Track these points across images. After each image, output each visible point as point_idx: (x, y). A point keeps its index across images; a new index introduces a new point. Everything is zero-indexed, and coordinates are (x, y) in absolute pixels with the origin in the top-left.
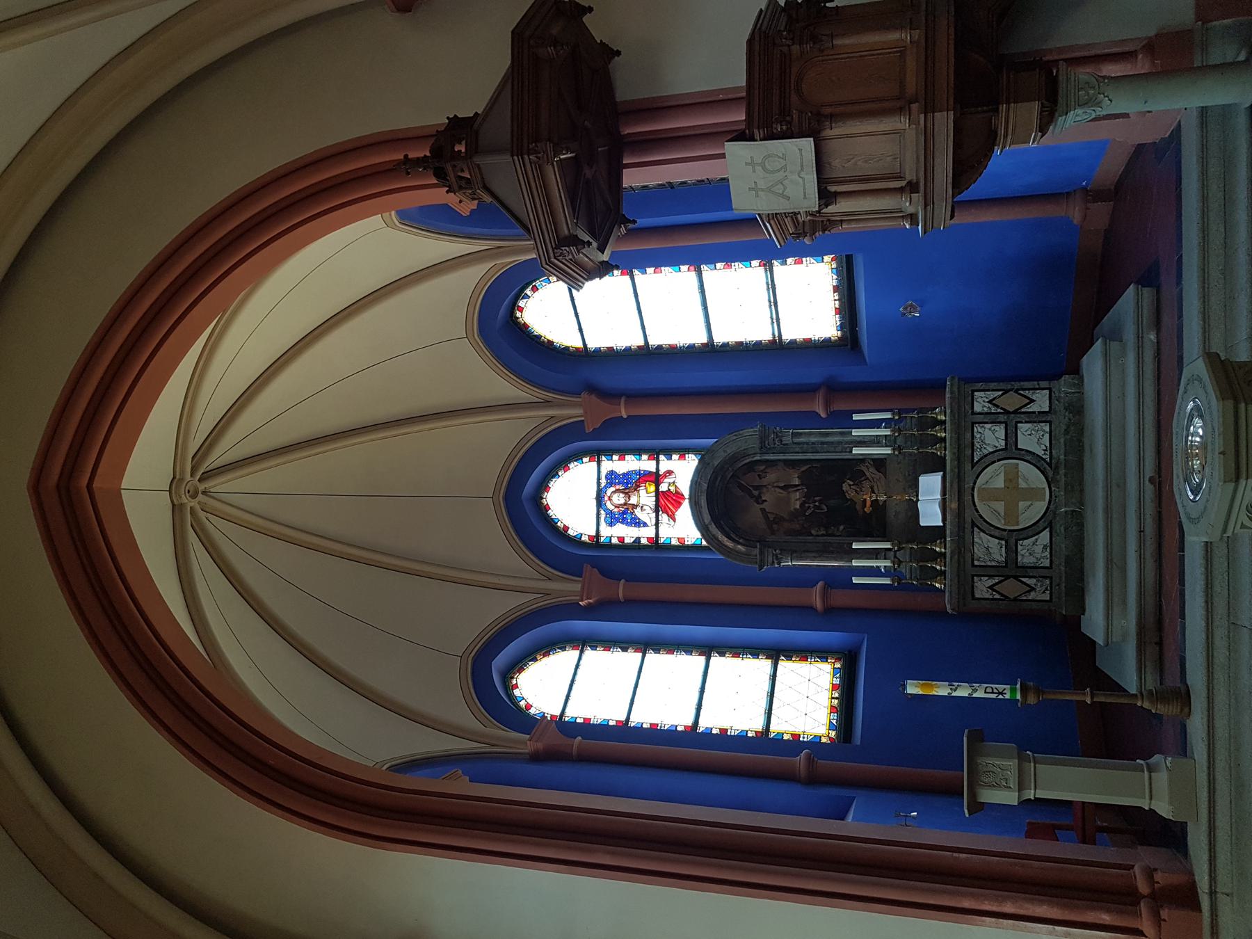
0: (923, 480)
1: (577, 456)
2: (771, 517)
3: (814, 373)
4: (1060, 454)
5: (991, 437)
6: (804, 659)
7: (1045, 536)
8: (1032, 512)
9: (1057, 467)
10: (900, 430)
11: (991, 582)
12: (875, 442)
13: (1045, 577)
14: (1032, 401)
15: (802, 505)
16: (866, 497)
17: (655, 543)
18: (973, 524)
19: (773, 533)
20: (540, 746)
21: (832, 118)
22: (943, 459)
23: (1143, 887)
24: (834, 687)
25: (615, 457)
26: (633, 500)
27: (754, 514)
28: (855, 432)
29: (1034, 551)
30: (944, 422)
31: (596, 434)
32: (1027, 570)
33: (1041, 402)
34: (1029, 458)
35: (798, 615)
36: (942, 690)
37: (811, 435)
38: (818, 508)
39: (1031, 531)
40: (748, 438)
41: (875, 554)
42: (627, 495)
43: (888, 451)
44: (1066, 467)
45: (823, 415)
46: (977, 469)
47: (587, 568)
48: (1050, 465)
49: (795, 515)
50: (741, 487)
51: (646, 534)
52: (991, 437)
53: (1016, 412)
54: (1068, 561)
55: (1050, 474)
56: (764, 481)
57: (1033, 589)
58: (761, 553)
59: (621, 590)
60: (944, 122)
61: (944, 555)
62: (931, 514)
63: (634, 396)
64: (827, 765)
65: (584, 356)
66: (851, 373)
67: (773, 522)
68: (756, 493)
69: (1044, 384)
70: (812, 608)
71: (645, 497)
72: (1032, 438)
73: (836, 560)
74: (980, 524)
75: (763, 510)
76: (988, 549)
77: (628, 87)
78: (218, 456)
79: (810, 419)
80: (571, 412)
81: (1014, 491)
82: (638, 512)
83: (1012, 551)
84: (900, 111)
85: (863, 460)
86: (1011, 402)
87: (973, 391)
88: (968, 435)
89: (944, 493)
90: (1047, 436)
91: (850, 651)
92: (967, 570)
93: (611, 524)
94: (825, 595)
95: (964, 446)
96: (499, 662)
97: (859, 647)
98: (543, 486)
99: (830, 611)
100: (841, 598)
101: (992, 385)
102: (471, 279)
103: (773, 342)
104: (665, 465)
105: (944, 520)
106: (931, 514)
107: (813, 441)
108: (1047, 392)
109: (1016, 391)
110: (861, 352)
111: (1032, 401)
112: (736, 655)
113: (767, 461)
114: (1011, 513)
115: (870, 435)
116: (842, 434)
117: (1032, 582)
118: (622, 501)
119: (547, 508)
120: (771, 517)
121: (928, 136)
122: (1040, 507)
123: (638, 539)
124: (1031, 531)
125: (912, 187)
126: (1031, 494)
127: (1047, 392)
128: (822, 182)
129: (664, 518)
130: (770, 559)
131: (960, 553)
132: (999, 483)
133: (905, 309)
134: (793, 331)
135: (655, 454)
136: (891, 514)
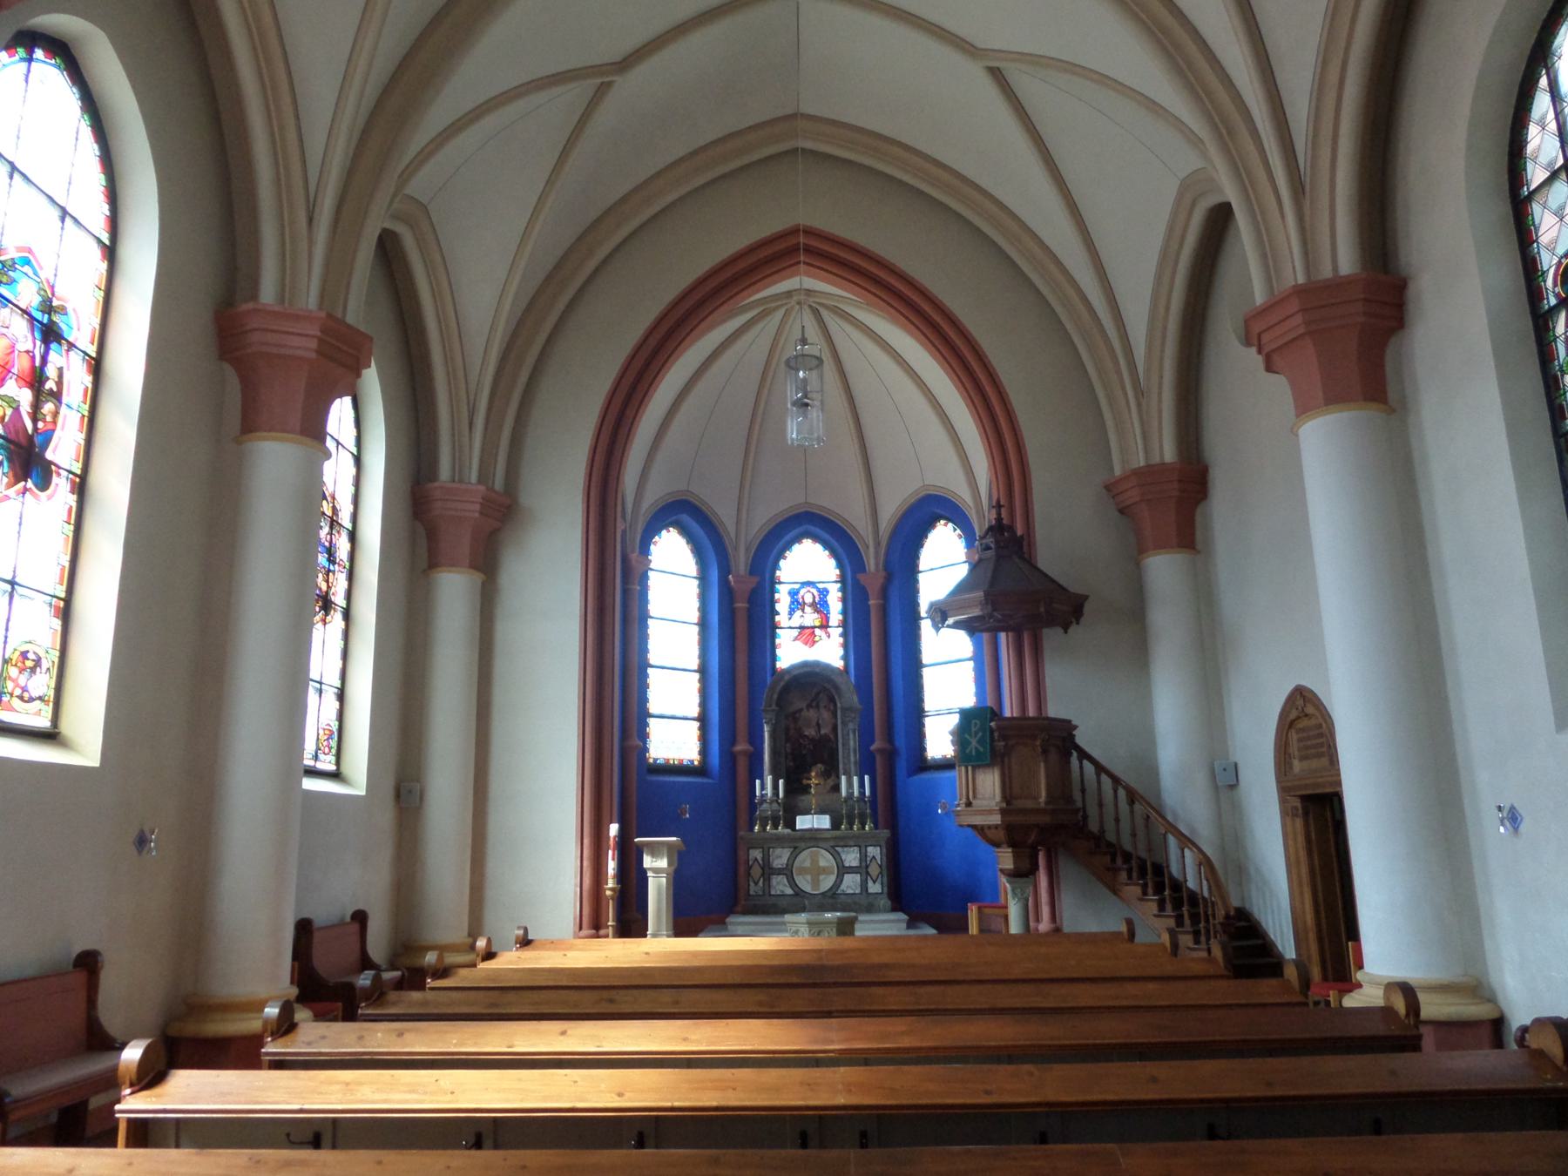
1: (840, 565)
3: (901, 742)
5: (851, 857)
7: (789, 891)
8: (805, 884)
17: (775, 627)
26: (807, 609)
29: (780, 885)
31: (856, 582)
32: (768, 880)
35: (729, 736)
42: (813, 605)
45: (873, 748)
47: (755, 580)
49: (799, 731)
50: (818, 694)
52: (851, 857)
54: (774, 905)
56: (823, 711)
59: (741, 605)
62: (803, 822)
63: (884, 610)
64: (634, 761)
66: (902, 765)
67: (795, 716)
71: (811, 618)
78: (825, 313)
79: (866, 736)
81: (817, 871)
82: (799, 613)
83: (780, 872)
86: (874, 870)
92: (767, 844)
95: (845, 842)
96: (685, 518)
98: (816, 539)
102: (963, 494)
106: (803, 822)
107: (849, 747)
114: (803, 871)
115: (852, 785)
121: (990, 812)
122: (807, 888)
125: (969, 804)
126: (816, 883)
129: (796, 632)
132: (822, 863)
135: (844, 624)
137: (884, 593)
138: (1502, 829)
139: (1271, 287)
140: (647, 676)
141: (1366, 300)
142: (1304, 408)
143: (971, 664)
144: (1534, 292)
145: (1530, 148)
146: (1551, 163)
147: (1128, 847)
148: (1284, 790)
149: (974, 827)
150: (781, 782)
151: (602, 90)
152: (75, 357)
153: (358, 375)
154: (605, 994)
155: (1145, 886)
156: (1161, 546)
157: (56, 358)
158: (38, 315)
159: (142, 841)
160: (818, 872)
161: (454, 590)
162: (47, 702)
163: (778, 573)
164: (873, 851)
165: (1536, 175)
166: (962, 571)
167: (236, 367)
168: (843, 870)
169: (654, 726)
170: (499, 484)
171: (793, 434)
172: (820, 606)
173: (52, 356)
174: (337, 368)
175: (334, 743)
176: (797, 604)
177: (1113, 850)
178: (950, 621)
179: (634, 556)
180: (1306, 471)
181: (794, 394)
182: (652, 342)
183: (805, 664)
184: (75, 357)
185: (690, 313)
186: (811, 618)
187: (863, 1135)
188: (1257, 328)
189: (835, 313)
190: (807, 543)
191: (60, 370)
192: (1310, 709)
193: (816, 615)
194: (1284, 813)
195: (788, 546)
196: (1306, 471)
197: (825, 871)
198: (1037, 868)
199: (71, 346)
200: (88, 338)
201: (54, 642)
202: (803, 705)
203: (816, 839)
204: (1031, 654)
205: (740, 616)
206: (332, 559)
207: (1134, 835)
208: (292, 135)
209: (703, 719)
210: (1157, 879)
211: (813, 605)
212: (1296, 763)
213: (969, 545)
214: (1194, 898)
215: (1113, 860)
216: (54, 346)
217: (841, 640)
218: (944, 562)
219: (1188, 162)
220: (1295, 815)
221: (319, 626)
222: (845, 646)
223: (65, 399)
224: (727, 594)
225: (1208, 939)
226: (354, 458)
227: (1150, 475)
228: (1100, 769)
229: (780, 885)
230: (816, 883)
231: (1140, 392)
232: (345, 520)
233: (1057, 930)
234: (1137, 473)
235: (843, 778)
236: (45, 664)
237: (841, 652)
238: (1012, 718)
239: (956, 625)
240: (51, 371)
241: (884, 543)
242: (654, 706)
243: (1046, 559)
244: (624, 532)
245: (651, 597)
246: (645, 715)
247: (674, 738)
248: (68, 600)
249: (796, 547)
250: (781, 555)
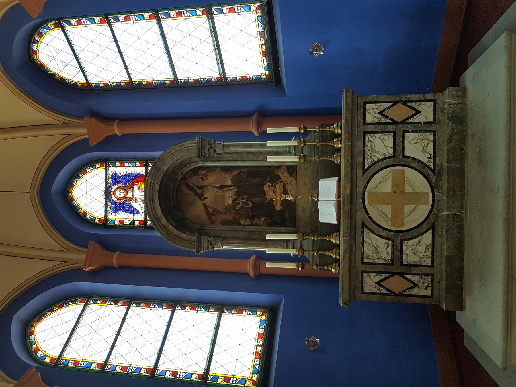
1: (91, 163)
2: (211, 211)
3: (250, 102)
4: (442, 160)
5: (381, 145)
6: (240, 312)
8: (416, 215)
9: (440, 174)
10: (305, 142)
11: (378, 278)
12: (287, 151)
13: (427, 275)
14: (418, 112)
15: (234, 201)
16: (275, 195)
18: (364, 225)
19: (212, 223)
22: (339, 166)
24: (260, 336)
25: (118, 164)
26: (130, 195)
28: (269, 143)
29: (417, 251)
30: (339, 135)
34: (413, 165)
37: (238, 147)
38: (246, 203)
39: (415, 232)
40: (188, 150)
41: (286, 243)
42: (126, 191)
43: (295, 159)
44: (450, 174)
46: (368, 174)
48: (433, 171)
49: (228, 209)
50: (189, 187)
52: (381, 145)
53: (403, 122)
54: (449, 261)
55: (434, 179)
56: (206, 183)
57: (415, 285)
58: (199, 240)
59: (115, 259)
61: (338, 246)
62: (328, 214)
63: (124, 120)
65: (88, 90)
66: (275, 103)
68: (199, 192)
69: (429, 96)
70: (247, 274)
73: (256, 245)
74: (369, 225)
75: (205, 205)
76: (377, 248)
79: (247, 136)
80: (80, 132)
81: (399, 196)
83: (398, 250)
85: (278, 167)
86: (400, 113)
87: (365, 103)
88: (361, 144)
89: (339, 195)
90: (431, 145)
91: (273, 307)
92: (358, 268)
93: (115, 212)
97: (279, 304)
101: (382, 98)
103: (219, 80)
105: (338, 220)
106: (328, 214)
107: (237, 152)
108: (432, 104)
109: (404, 103)
110: (284, 91)
111: (418, 112)
112: (193, 308)
113: (208, 167)
114: (397, 215)
115: (281, 148)
116: (261, 145)
117: (415, 279)
118: (122, 195)
119: (72, 199)
120: (211, 211)
122: (423, 210)
123: (133, 222)
124: (415, 232)
126: (416, 198)
127: (432, 104)
130: (206, 245)
131: (351, 251)
132: (387, 188)
133: (313, 49)
134: (235, 71)
136: (299, 209)
137: (107, 119)
150: (269, 237)
160: (400, 194)
164: (372, 114)
168: (399, 158)
187: (397, 185)
197: (398, 185)
202: (199, 203)
203: (352, 195)
224: (101, 273)
230: (416, 198)
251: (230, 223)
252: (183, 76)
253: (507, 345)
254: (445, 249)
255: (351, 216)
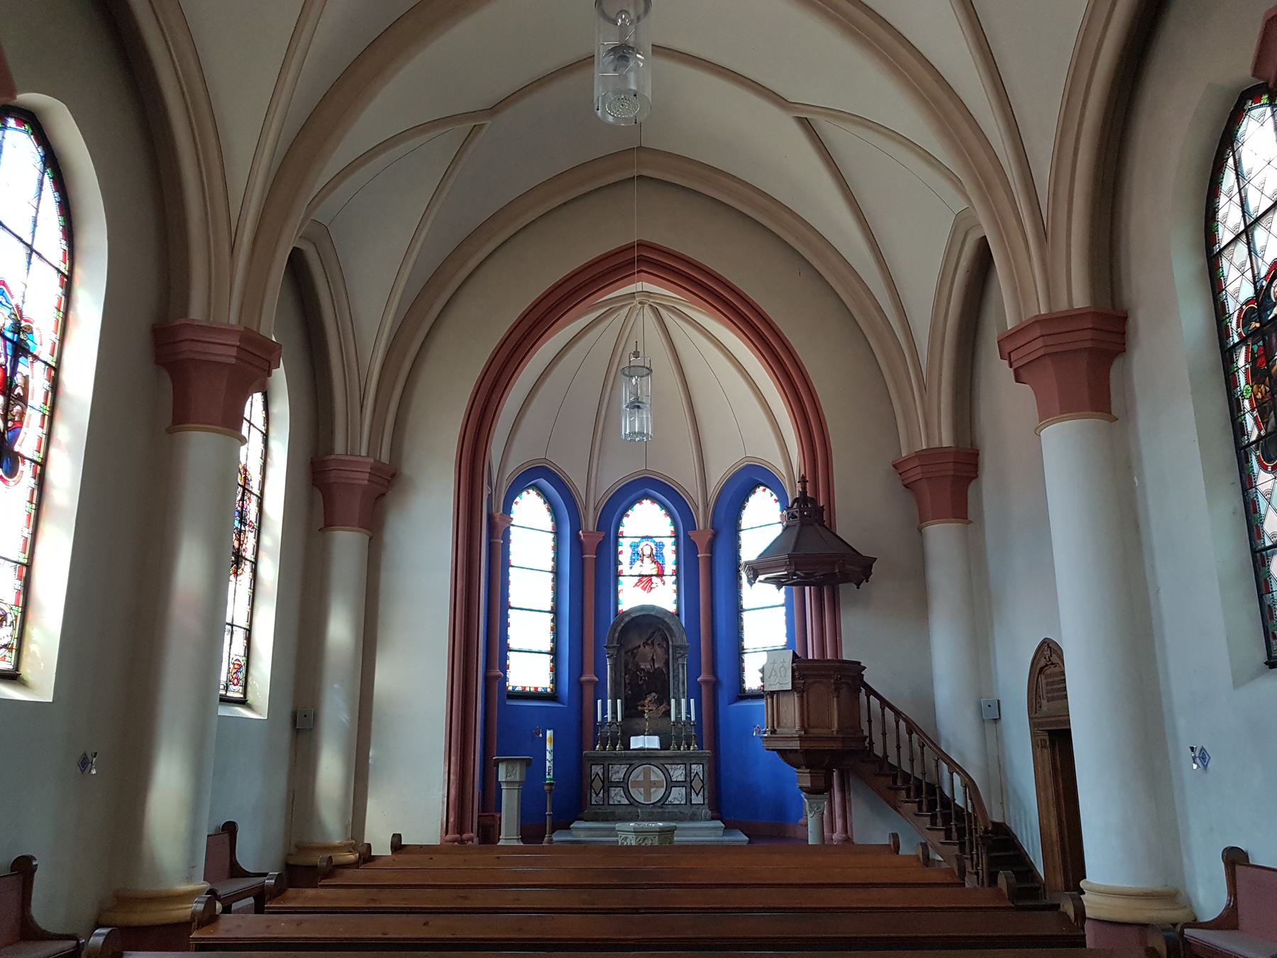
0: (657, 738)
4: (670, 809)
5: (678, 774)
17: (618, 575)
20: (497, 520)
21: (801, 698)
23: (465, 836)
27: (637, 641)
29: (617, 796)
33: (697, 800)
35: (578, 665)
36: (549, 747)
37: (683, 674)
39: (628, 794)
41: (615, 712)
42: (651, 556)
49: (637, 666)
51: (624, 568)
52: (678, 774)
59: (590, 556)
60: (796, 745)
62: (636, 742)
63: (711, 561)
65: (736, 529)
66: (724, 695)
67: (633, 653)
70: (581, 675)
71: (649, 568)
72: (677, 795)
76: (618, 773)
77: (846, 590)
79: (694, 670)
81: (649, 786)
82: (638, 563)
83: (617, 784)
84: (802, 726)
85: (669, 704)
86: (697, 784)
92: (606, 761)
94: (590, 681)
95: (674, 760)
96: (543, 482)
98: (655, 500)
99: (581, 685)
100: (589, 692)
102: (779, 466)
104: (670, 580)
106: (636, 742)
107: (681, 674)
110: (736, 701)
114: (637, 784)
115: (683, 709)
119: (640, 503)
121: (791, 738)
123: (621, 563)
124: (628, 794)
125: (773, 732)
126: (648, 795)
128: (778, 692)
132: (653, 778)
135: (676, 573)
136: (637, 720)
138: (1195, 766)
139: (1020, 314)
140: (507, 616)
141: (1092, 328)
142: (1046, 415)
143: (784, 609)
144: (1223, 332)
145: (1221, 214)
146: (1237, 226)
147: (906, 768)
148: (1034, 724)
149: (779, 751)
151: (476, 130)
152: (39, 366)
153: (269, 374)
154: (462, 892)
155: (920, 803)
156: (939, 517)
157: (23, 367)
158: (9, 335)
159: (84, 763)
160: (649, 785)
161: (346, 545)
162: (10, 650)
163: (621, 529)
164: (696, 768)
165: (1225, 236)
166: (778, 530)
167: (171, 371)
169: (513, 659)
170: (385, 458)
171: (626, 429)
172: (656, 558)
173: (21, 368)
174: (251, 373)
175: (241, 676)
176: (637, 556)
177: (894, 772)
178: (761, 577)
179: (498, 514)
180: (1051, 460)
181: (626, 397)
182: (516, 337)
183: (642, 608)
184: (39, 366)
185: (551, 310)
186: (649, 568)
188: (1008, 348)
189: (673, 312)
190: (647, 503)
191: (26, 378)
192: (1055, 659)
193: (653, 565)
194: (1035, 746)
195: (630, 506)
196: (1051, 460)
197: (655, 784)
198: (831, 786)
199: (36, 358)
200: (49, 350)
201: (17, 600)
204: (829, 605)
205: (588, 562)
206: (243, 521)
207: (912, 760)
208: (218, 183)
209: (555, 652)
210: (928, 798)
211: (651, 556)
212: (1044, 702)
213: (784, 507)
214: (960, 811)
215: (895, 782)
216: (22, 359)
217: (674, 587)
218: (762, 522)
219: (961, 205)
220: (1043, 747)
221: (232, 577)
222: (678, 591)
223: (30, 402)
225: (972, 850)
226: (265, 447)
227: (929, 457)
228: (884, 703)
229: (617, 796)
231: (923, 387)
232: (254, 486)
233: (848, 840)
234: (920, 455)
235: (673, 701)
236: (10, 618)
237: (674, 596)
238: (813, 660)
239: (767, 580)
240: (19, 379)
241: (712, 504)
242: (513, 642)
243: (844, 528)
244: (490, 496)
245: (511, 549)
246: (506, 648)
247: (529, 670)
248: (29, 566)
249: (637, 506)
250: (624, 513)
251: (626, 667)
252: (745, 615)
253: (1010, 268)
254: (619, 811)
255: (636, 757)
